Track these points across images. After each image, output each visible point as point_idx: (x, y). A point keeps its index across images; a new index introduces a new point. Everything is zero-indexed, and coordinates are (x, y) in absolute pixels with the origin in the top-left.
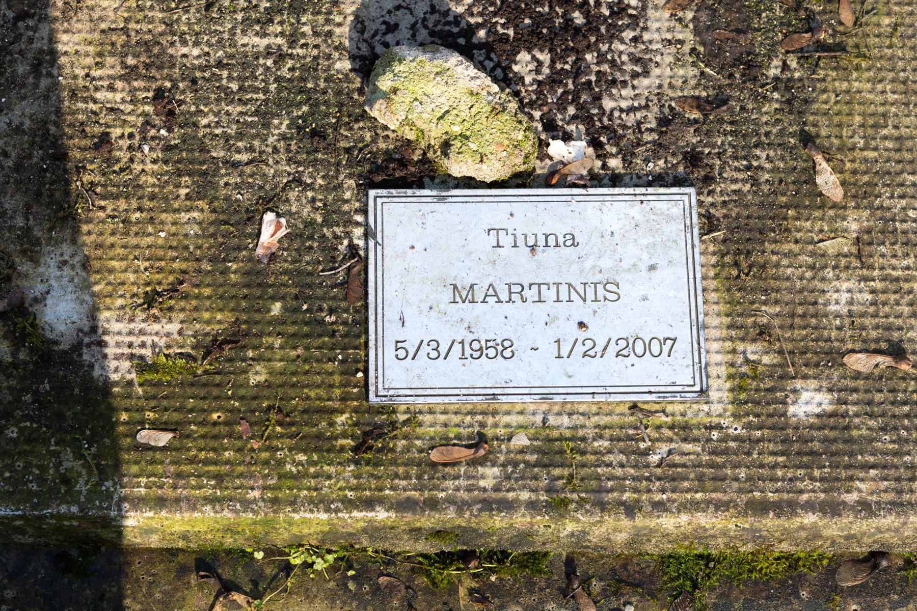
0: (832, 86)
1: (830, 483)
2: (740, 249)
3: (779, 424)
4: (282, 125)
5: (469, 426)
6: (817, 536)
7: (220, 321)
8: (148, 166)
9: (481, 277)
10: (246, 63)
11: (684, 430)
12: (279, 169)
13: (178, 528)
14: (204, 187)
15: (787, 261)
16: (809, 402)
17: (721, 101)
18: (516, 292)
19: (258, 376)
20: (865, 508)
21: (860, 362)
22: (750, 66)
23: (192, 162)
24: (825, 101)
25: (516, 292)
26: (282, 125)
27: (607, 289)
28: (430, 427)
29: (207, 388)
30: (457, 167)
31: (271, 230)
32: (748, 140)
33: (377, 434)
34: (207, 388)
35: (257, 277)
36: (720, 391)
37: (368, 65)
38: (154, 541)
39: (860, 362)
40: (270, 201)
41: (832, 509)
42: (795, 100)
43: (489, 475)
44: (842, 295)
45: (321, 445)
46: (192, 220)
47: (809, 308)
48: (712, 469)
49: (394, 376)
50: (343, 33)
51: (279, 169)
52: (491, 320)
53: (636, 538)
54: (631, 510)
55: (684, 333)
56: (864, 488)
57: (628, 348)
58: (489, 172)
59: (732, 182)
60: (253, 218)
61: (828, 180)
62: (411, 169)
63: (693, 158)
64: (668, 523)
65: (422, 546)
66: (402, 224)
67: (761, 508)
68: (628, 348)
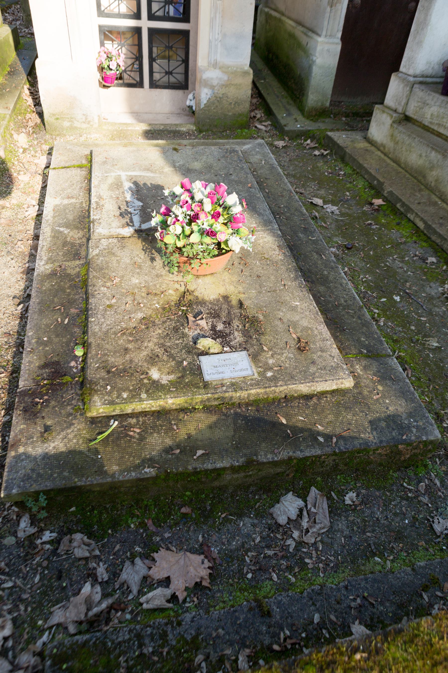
0: (263, 339)
1: (275, 383)
2: (255, 358)
3: (266, 377)
4: (184, 351)
5: (220, 382)
6: (275, 392)
7: (180, 375)
8: (165, 358)
9: (218, 365)
10: (177, 344)
11: (252, 380)
12: (184, 356)
13: (178, 402)
14: (174, 359)
15: (262, 358)
16: (269, 374)
17: (247, 341)
18: (224, 366)
19: (187, 380)
20: (281, 386)
21: (276, 368)
22: (251, 337)
23: (171, 356)
24: (263, 340)
25: (224, 366)
26: (184, 351)
27: (236, 364)
28: (214, 383)
29: (180, 383)
30: (212, 351)
31: (185, 363)
32: (252, 345)
33: (206, 385)
34: (180, 383)
35: (184, 369)
36: (256, 375)
37: (195, 343)
38: (174, 407)
39: (276, 368)
40: (185, 359)
41: (277, 386)
42: (258, 340)
43: (224, 388)
44: (271, 361)
45: (199, 387)
46: (173, 363)
47: (267, 363)
48: (257, 384)
49: (207, 377)
50: (191, 339)
51: (184, 356)
52: (220, 369)
53: (249, 395)
54: (247, 390)
55: (249, 368)
56: (280, 383)
57: (241, 370)
58: (216, 351)
59: (251, 350)
60: (182, 362)
61: (265, 348)
62: (205, 353)
63: (245, 348)
64: (253, 391)
65: (216, 403)
66: (205, 361)
67: (266, 387)
68: (241, 370)
